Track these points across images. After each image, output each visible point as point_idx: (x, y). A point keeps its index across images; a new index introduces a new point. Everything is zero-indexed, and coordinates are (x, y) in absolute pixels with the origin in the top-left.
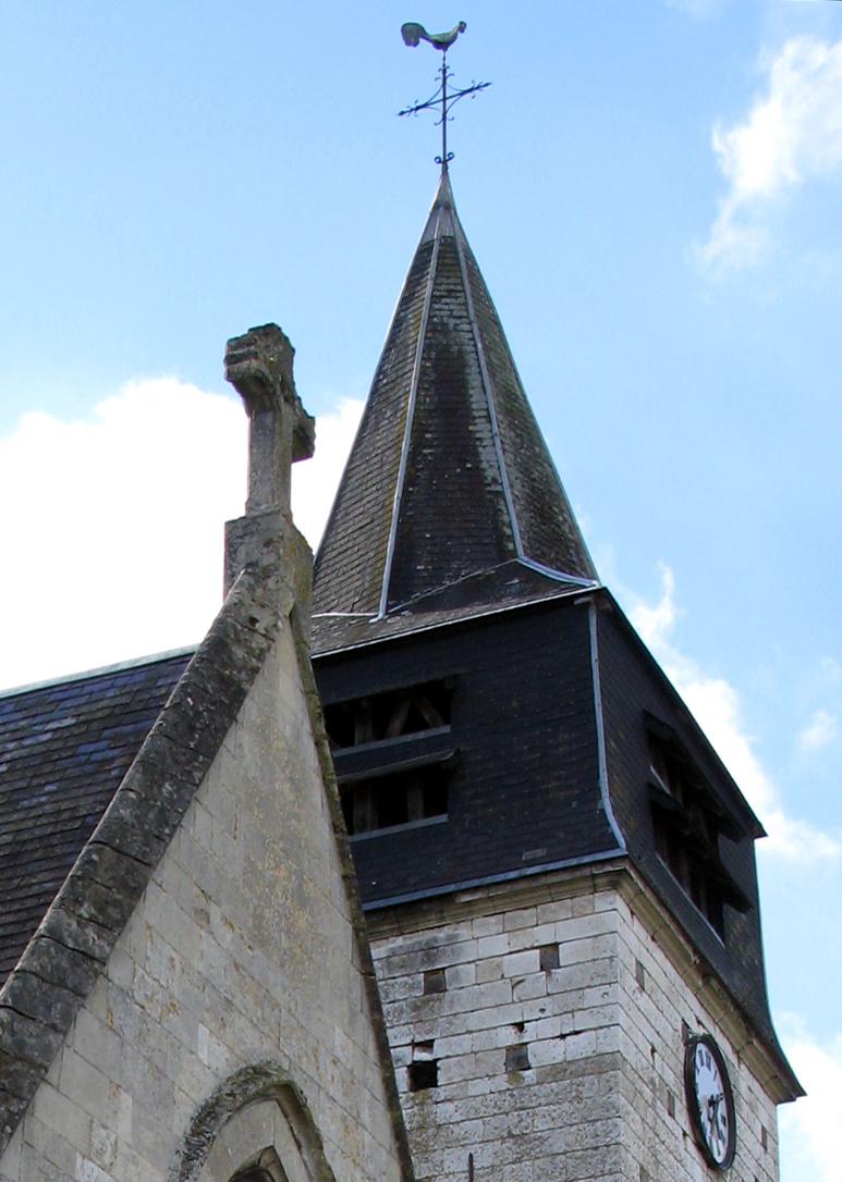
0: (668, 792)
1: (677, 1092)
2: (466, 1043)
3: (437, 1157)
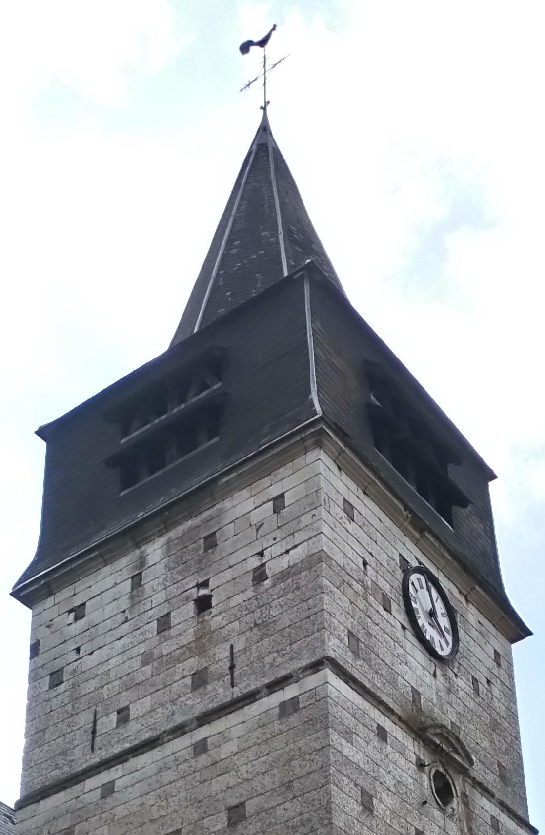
0: (378, 404)
1: (394, 598)
2: (229, 575)
3: (211, 653)
